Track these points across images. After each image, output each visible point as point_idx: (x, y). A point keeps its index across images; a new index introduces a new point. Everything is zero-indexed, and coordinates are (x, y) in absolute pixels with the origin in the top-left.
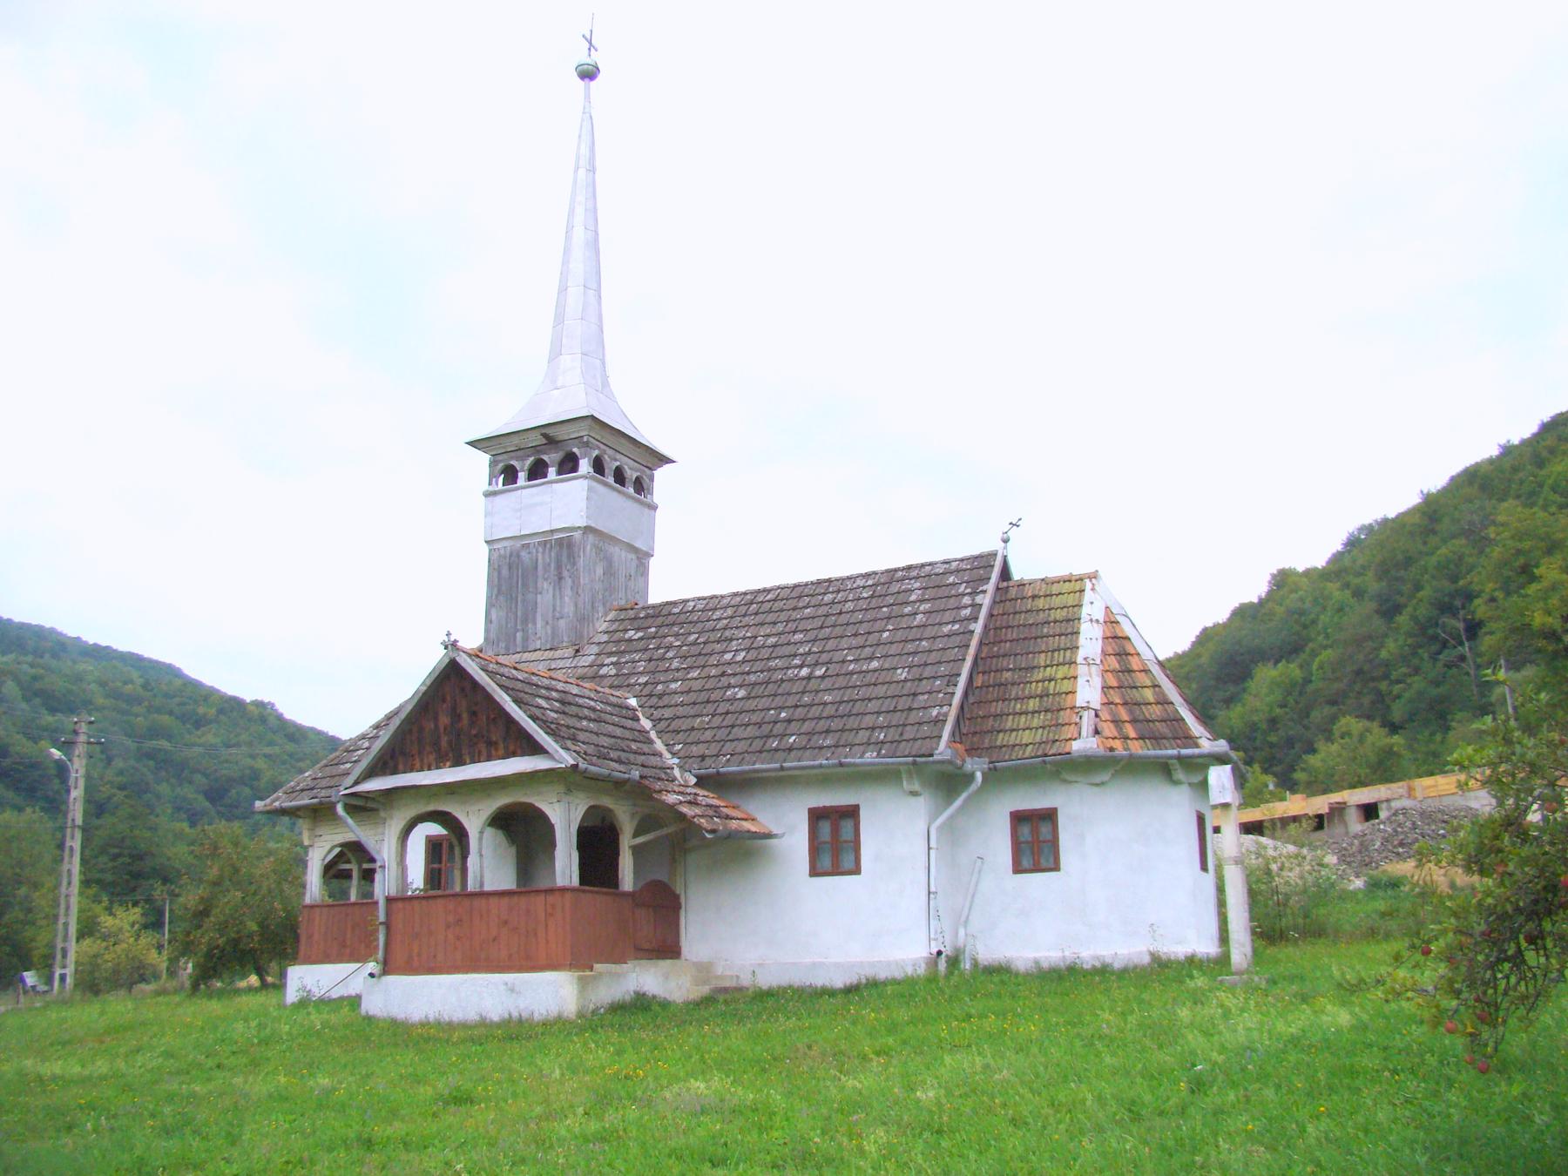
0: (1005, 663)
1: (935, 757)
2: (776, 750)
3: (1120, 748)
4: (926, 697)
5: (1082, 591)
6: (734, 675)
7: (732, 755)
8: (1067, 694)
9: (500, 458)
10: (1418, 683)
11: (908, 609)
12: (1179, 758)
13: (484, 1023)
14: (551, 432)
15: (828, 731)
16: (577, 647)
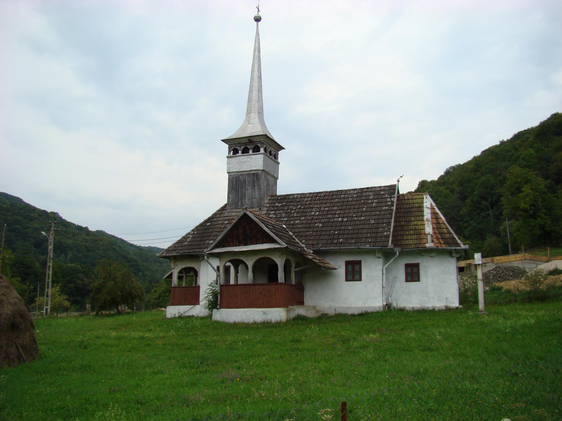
1: (388, 247)
2: (337, 243)
3: (439, 246)
4: (382, 229)
5: (423, 198)
6: (317, 219)
9: (232, 146)
10: (473, 223)
11: (370, 201)
12: (456, 250)
13: (255, 323)
14: (251, 139)
15: (352, 238)
16: (260, 208)
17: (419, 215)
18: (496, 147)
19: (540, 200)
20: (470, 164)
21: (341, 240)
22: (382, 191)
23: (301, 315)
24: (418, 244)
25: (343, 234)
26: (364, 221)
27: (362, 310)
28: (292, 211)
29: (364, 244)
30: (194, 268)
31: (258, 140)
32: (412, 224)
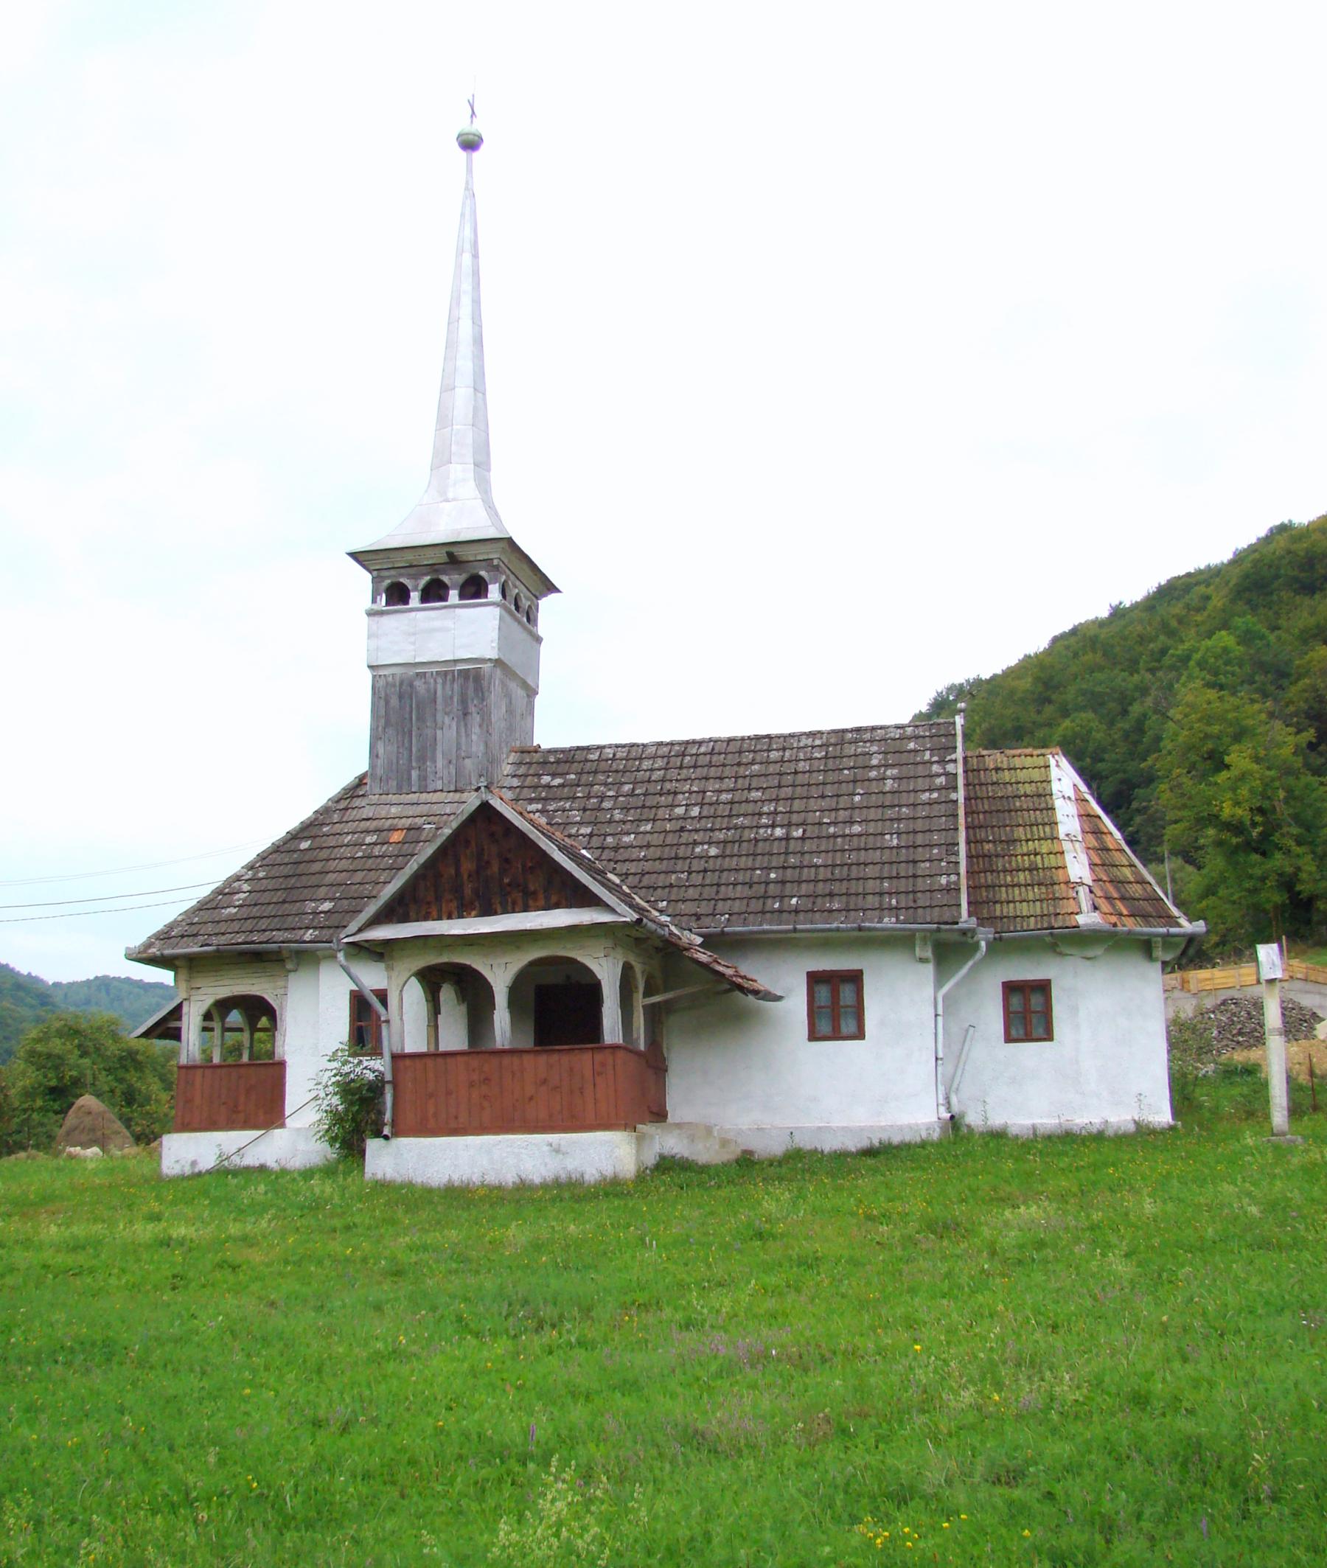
0: (983, 835)
1: (960, 925)
2: (780, 911)
4: (928, 864)
6: (697, 831)
7: (730, 914)
8: (1056, 868)
11: (873, 774)
15: (831, 895)
17: (1040, 821)
18: (1100, 624)
19: (1282, 794)
20: (1019, 678)
21: (794, 901)
22: (909, 738)
23: (673, 1157)
24: (1048, 915)
25: (800, 882)
26: (863, 838)
27: (869, 1138)
28: (602, 802)
29: (877, 913)
30: (263, 999)
31: (479, 558)
32: (1019, 851)
